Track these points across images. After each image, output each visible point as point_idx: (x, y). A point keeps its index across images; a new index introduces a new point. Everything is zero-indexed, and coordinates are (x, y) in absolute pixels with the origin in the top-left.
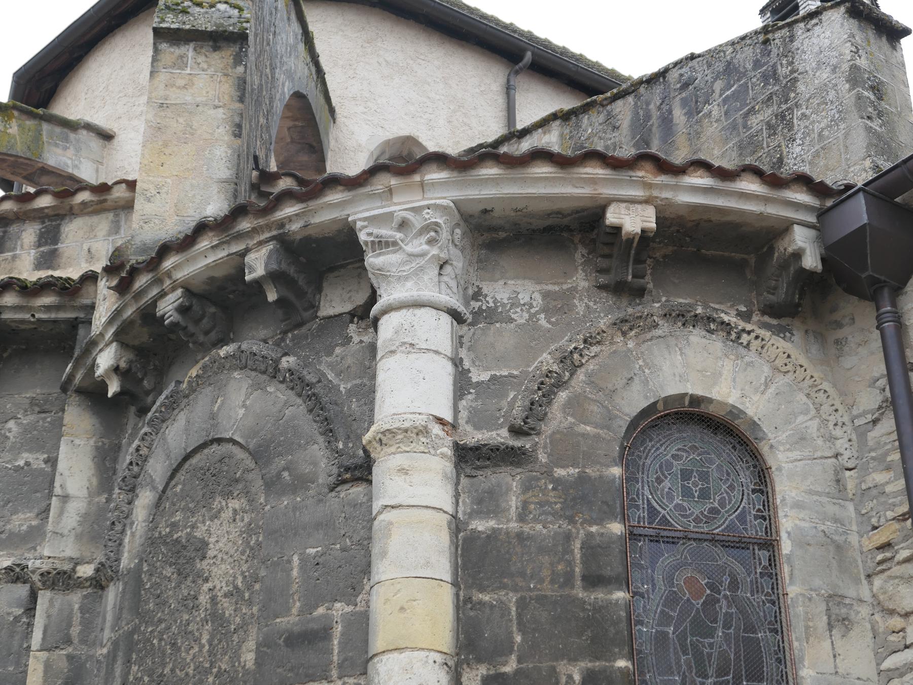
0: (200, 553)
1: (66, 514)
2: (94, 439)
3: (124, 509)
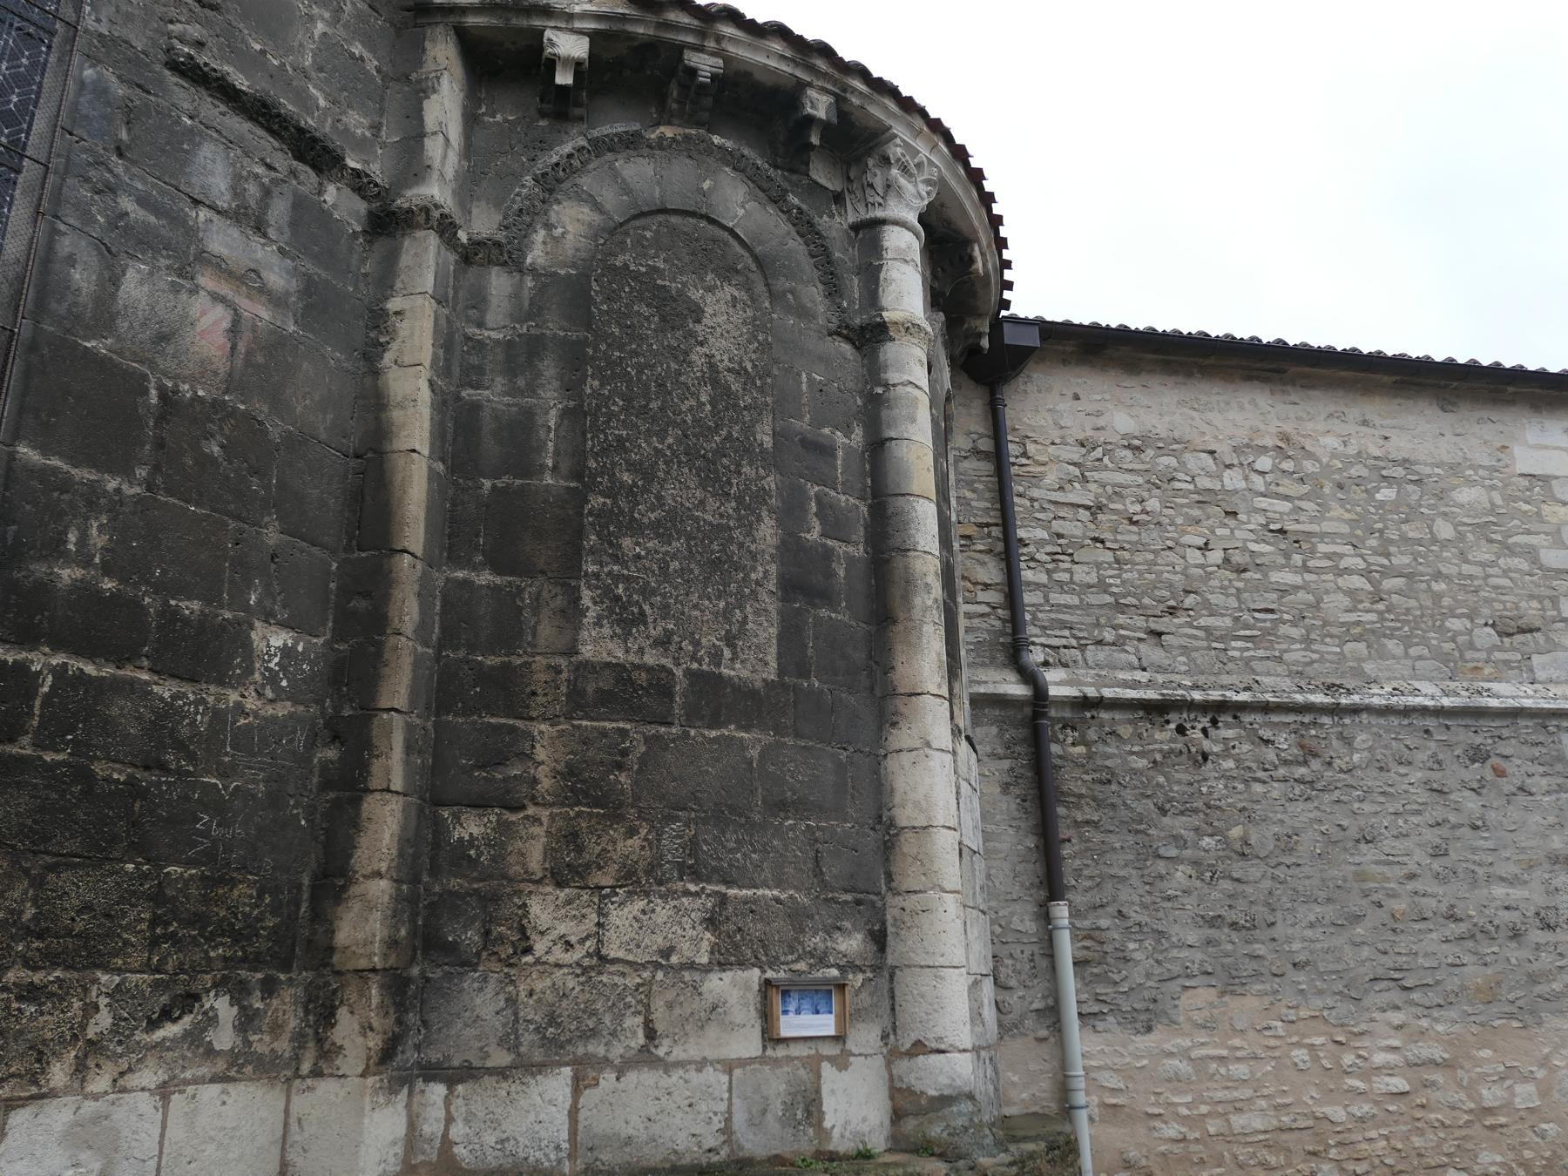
2: (1006, 764)
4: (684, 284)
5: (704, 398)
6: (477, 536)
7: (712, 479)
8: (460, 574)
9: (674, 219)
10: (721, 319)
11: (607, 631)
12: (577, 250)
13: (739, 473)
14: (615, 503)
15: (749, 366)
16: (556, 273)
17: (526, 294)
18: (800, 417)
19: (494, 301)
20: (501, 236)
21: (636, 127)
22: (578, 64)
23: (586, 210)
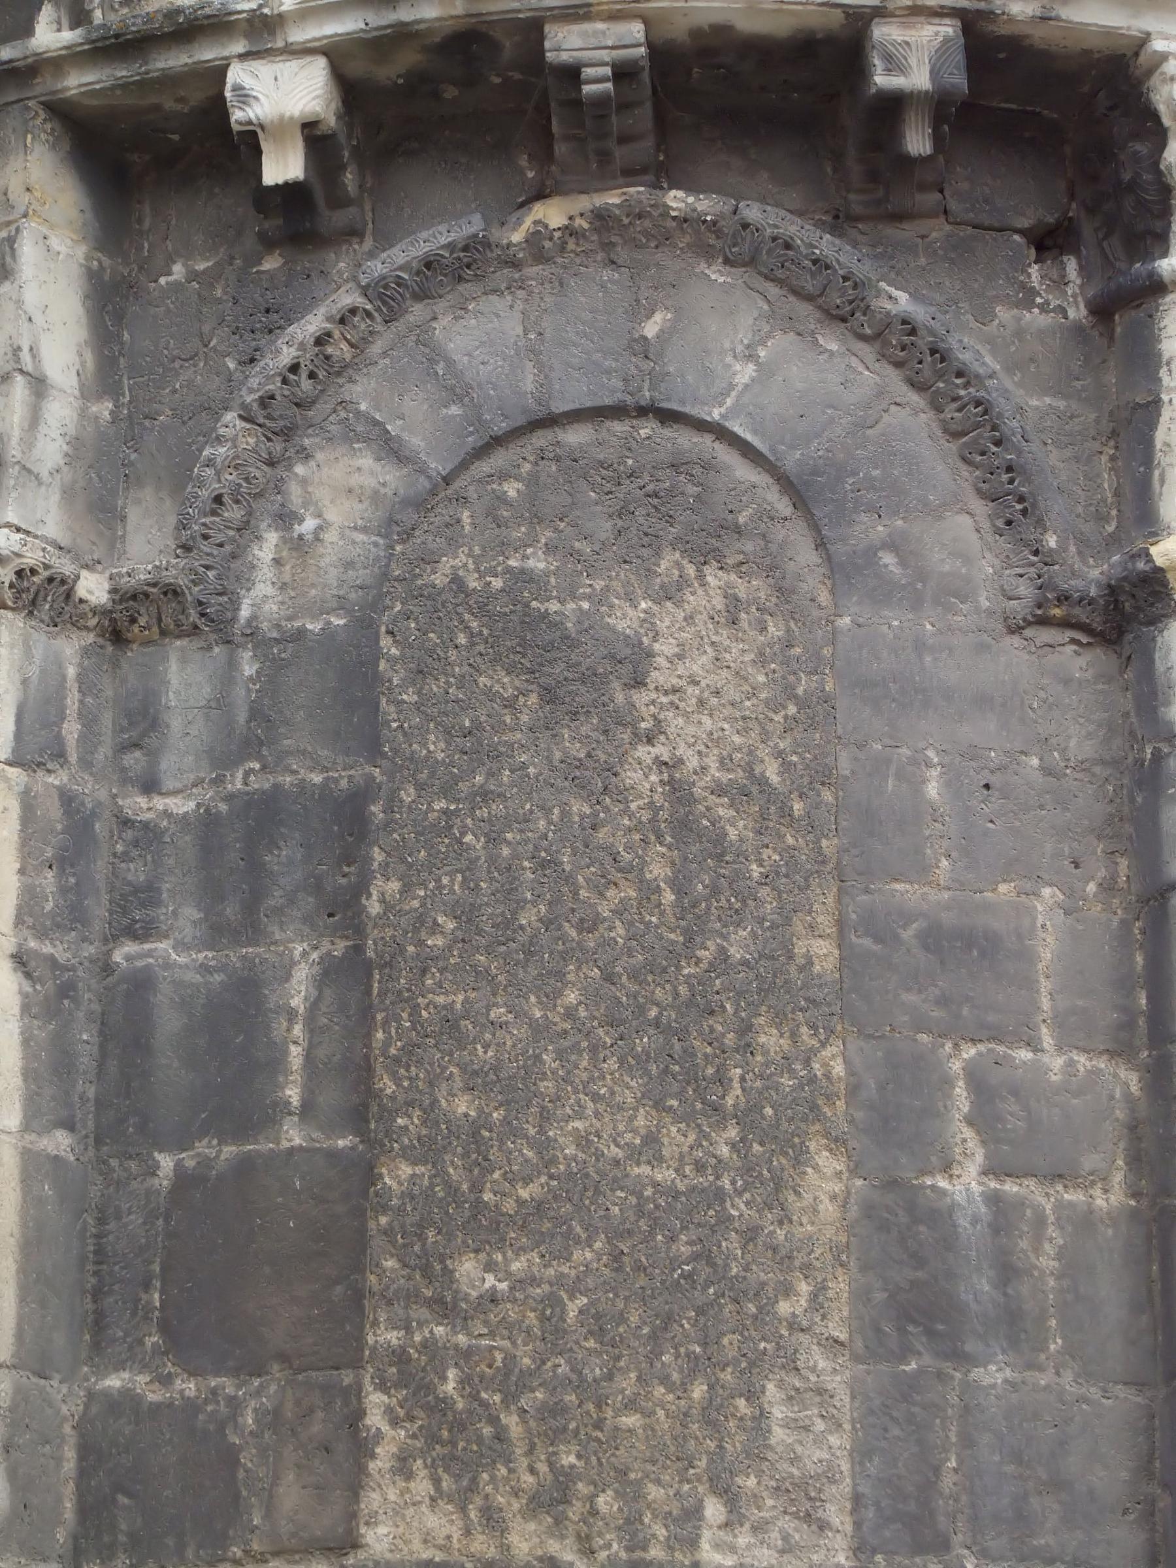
0: (625, 670)
1: (43, 429)
3: (254, 472)
4: (598, 599)
5: (658, 871)
6: (147, 1286)
7: (682, 1082)
8: (114, 1382)
9: (575, 436)
10: (698, 665)
11: (422, 1486)
12: (349, 565)
13: (748, 1049)
14: (439, 1173)
15: (772, 772)
16: (301, 633)
17: (241, 696)
18: (922, 871)
19: (176, 723)
20: (176, 572)
21: (473, 225)
22: (310, 129)
23: (366, 461)
